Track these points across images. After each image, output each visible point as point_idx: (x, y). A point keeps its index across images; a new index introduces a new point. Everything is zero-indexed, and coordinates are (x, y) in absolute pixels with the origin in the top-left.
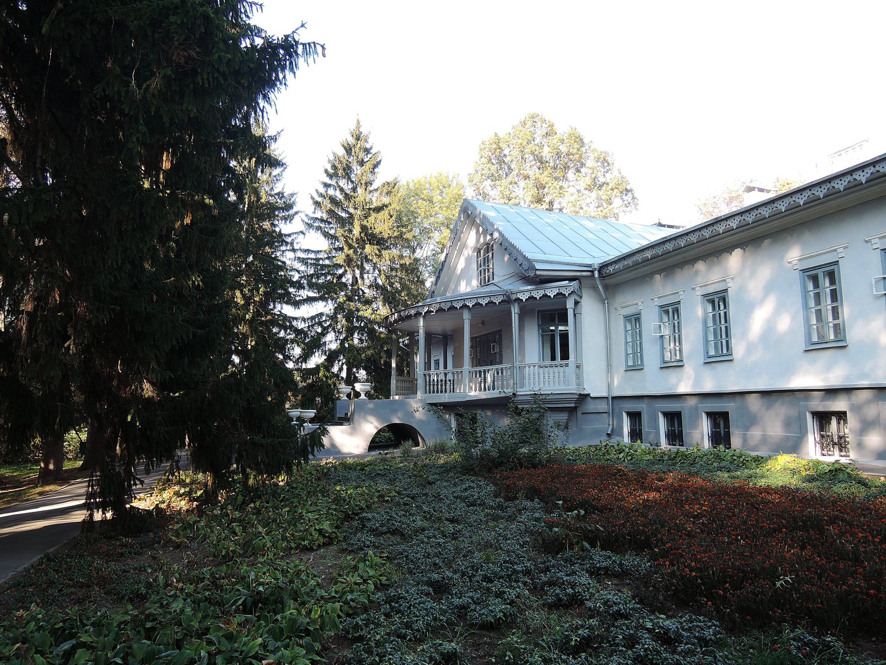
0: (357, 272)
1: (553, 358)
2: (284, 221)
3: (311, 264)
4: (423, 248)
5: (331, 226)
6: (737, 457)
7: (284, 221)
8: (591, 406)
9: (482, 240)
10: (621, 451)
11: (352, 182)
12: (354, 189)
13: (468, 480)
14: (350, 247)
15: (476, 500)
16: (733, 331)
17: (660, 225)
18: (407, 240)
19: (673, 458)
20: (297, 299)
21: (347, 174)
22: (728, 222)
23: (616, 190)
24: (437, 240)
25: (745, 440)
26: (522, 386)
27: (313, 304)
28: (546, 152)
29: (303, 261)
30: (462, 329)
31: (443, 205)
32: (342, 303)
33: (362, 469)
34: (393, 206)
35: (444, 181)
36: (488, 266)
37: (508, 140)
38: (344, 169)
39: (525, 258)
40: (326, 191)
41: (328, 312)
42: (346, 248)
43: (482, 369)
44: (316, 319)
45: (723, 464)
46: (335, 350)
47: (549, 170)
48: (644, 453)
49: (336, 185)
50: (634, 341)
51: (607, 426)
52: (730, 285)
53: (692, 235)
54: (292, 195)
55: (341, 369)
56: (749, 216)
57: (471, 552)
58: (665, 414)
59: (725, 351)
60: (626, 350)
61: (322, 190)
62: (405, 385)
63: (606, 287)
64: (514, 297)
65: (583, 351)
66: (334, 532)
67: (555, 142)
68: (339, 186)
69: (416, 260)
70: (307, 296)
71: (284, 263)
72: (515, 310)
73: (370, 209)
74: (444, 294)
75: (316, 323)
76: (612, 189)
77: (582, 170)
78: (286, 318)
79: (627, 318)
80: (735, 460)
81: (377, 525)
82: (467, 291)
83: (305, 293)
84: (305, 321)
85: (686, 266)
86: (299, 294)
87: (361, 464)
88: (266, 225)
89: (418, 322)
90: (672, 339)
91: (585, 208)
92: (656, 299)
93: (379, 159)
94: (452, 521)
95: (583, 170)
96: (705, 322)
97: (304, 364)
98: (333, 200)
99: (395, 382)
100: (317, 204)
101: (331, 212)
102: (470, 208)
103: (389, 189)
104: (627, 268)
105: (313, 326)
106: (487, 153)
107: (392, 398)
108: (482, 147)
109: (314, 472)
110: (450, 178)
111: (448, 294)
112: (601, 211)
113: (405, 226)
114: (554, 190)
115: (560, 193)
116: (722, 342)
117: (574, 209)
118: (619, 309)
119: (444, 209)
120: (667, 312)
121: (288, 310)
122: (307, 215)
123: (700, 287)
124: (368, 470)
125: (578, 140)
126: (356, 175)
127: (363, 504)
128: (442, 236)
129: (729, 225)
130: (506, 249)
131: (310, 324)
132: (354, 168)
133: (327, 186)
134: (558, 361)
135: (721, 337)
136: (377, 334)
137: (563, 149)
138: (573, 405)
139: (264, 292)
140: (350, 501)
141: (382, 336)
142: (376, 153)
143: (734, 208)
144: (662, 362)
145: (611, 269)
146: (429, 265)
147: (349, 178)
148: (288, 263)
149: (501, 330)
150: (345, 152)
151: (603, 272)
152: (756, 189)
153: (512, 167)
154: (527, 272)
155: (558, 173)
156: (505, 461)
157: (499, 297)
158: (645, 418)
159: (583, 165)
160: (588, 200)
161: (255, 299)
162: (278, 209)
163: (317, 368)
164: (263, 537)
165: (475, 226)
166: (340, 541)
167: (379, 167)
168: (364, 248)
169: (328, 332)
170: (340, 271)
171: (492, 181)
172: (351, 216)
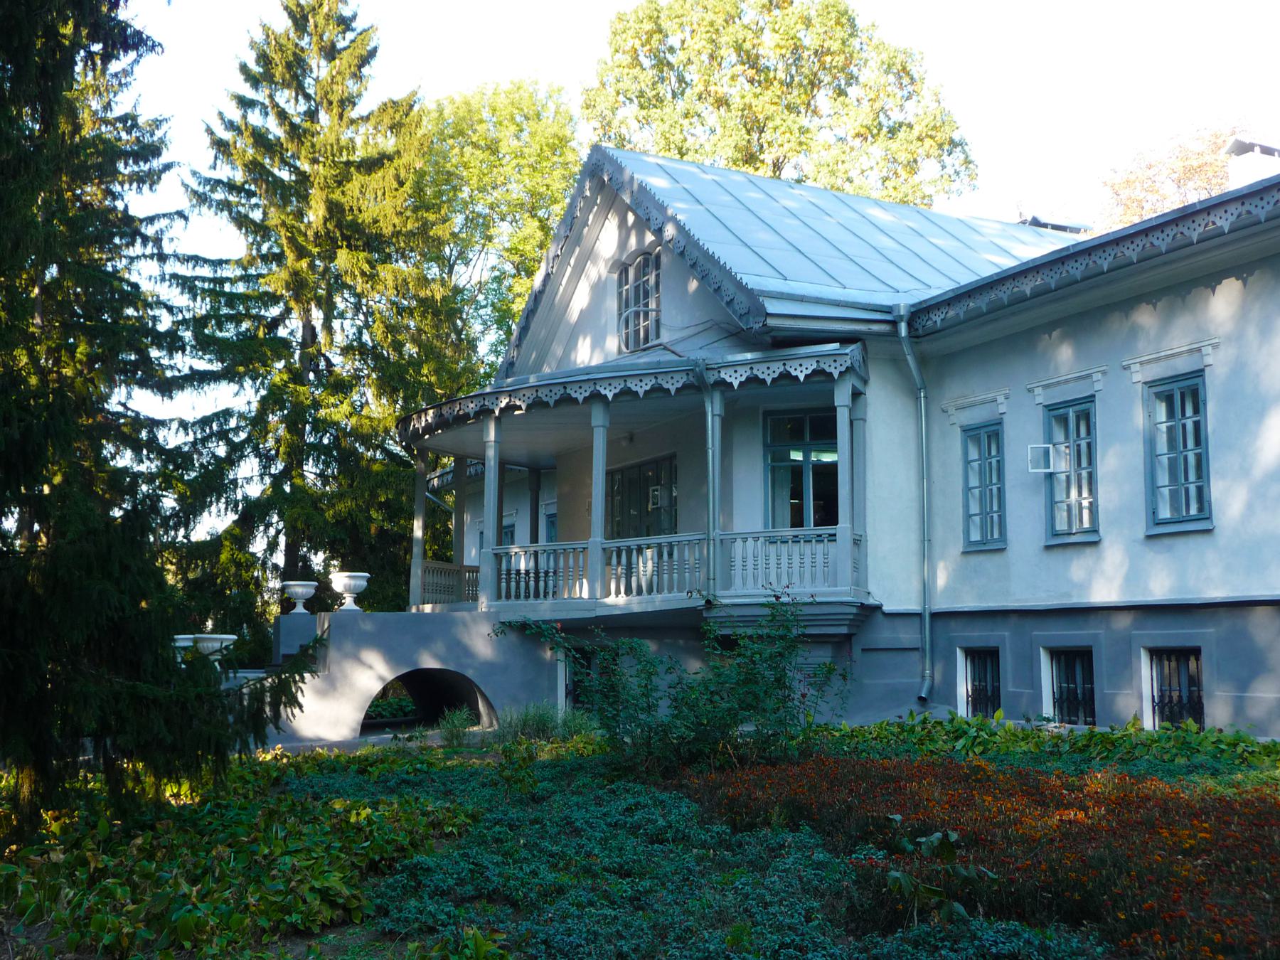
0: (317, 316)
1: (798, 521)
2: (135, 185)
3: (203, 290)
4: (472, 263)
5: (254, 200)
6: (1228, 745)
7: (135, 185)
8: (885, 635)
9: (633, 241)
10: (958, 734)
11: (308, 97)
12: (312, 115)
13: (627, 791)
14: (301, 253)
15: (663, 830)
16: (1214, 466)
17: (1036, 223)
18: (440, 242)
19: (1082, 749)
20: (169, 374)
21: (295, 77)
22: (1212, 218)
23: (928, 142)
24: (507, 245)
25: (1239, 707)
26: (728, 584)
27: (206, 388)
28: (769, 49)
29: (187, 284)
30: (586, 451)
31: (523, 162)
32: (278, 387)
33: (362, 771)
34: (405, 159)
35: (525, 105)
36: (647, 305)
37: (680, 12)
38: (289, 66)
39: (740, 286)
40: (244, 117)
41: (244, 409)
42: (290, 256)
43: (633, 542)
44: (216, 425)
45: (1199, 759)
46: (258, 499)
47: (776, 88)
48: (1014, 737)
49: (267, 102)
50: (983, 485)
51: (918, 680)
52: (1208, 360)
53: (1128, 244)
54: (157, 123)
55: (272, 546)
56: (1260, 204)
57: (691, 931)
58: (1055, 654)
59: (1193, 511)
60: (966, 506)
61: (235, 114)
62: (443, 580)
63: (922, 361)
64: (711, 378)
65: (869, 504)
66: (354, 896)
67: (792, 23)
68: (276, 106)
69: (457, 291)
70: (191, 368)
71: (135, 286)
72: (713, 409)
73: (348, 164)
74: (537, 367)
75: (212, 434)
76: (920, 139)
77: (849, 90)
78: (138, 422)
79: (971, 433)
80: (1223, 751)
81: (451, 882)
82: (594, 363)
83: (184, 362)
84: (186, 429)
85: (1194, 290)
86: (172, 362)
87: (359, 760)
88: (91, 192)
89: (482, 432)
90: (1073, 479)
91: (858, 180)
92: (1038, 391)
93: (372, 45)
94: (624, 873)
95: (853, 91)
96: (1150, 443)
97: (182, 532)
98: (260, 138)
99: (419, 572)
100: (221, 146)
101: (255, 168)
102: (607, 167)
103: (397, 117)
104: (975, 318)
105: (204, 440)
106: (631, 42)
107: (414, 610)
108: (620, 26)
109: (250, 777)
110: (541, 96)
111: (546, 370)
112: (895, 188)
113: (436, 208)
114: (788, 135)
115: (801, 144)
116: (1187, 491)
117: (833, 180)
118: (952, 410)
119: (527, 170)
120: (1064, 421)
121: (145, 402)
122: (194, 173)
123: (1141, 363)
124: (376, 774)
125: (844, 20)
126: (317, 80)
127: (403, 839)
128: (520, 235)
129: (1214, 223)
130: (694, 266)
131: (199, 436)
132: (313, 63)
133: (245, 103)
134: (810, 529)
135: (1186, 478)
136: (364, 463)
137: (810, 40)
138: (844, 630)
139: (87, 355)
140: (371, 832)
141: (376, 467)
142: (365, 31)
143: (1194, 195)
144: (1151, 523)
145: (937, 318)
146: (484, 303)
147: (300, 89)
148: (146, 286)
149: (672, 457)
150: (289, 23)
151: (917, 325)
152: (1257, 149)
153: (688, 79)
154: (744, 319)
155: (795, 97)
156: (707, 750)
157: (677, 377)
158: (1008, 663)
159: (852, 79)
160: (865, 163)
161: (64, 371)
162: (125, 155)
163: (215, 544)
164: (194, 905)
165: (615, 211)
166: (369, 916)
167: (372, 62)
168: (332, 258)
169: (242, 457)
170: (275, 311)
171: (642, 107)
172: (303, 178)
